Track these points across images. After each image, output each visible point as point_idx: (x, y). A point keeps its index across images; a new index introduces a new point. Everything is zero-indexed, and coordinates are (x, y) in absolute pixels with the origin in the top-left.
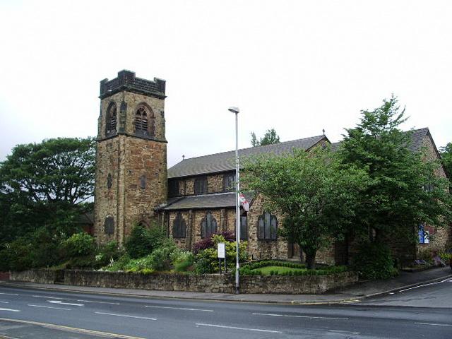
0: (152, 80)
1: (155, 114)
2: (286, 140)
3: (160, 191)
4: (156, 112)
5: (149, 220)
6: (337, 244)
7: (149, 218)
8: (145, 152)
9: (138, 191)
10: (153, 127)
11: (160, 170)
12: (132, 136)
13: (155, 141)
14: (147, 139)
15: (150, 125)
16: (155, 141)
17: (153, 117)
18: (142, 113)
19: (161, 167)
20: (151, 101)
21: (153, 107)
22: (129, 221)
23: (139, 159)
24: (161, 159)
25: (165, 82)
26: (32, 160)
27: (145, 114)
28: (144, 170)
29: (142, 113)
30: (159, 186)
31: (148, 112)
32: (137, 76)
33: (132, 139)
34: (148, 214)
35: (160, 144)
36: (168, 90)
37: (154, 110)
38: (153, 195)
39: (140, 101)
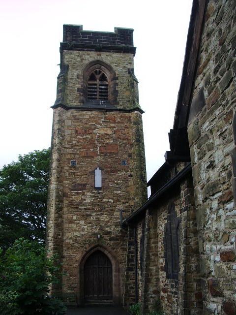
0: (113, 31)
1: (117, 73)
2: (101, 183)
3: (132, 192)
4: (119, 70)
5: (111, 243)
6: (175, 201)
7: (111, 239)
8: (100, 130)
9: (89, 194)
10: (116, 92)
11: (130, 155)
12: (77, 108)
13: (120, 111)
14: (103, 110)
15: (110, 90)
16: (120, 111)
17: (115, 78)
18: (98, 77)
19: (132, 150)
20: (107, 58)
21: (113, 65)
22: (70, 247)
23: (91, 142)
24: (132, 138)
25: (131, 31)
26: (13, 173)
27: (103, 78)
28: (99, 158)
29: (98, 77)
30: (131, 183)
31: (108, 75)
32: (85, 29)
33: (75, 113)
34: (110, 233)
35: (128, 114)
36: (137, 41)
37: (115, 68)
38: (118, 198)
39: (91, 60)
